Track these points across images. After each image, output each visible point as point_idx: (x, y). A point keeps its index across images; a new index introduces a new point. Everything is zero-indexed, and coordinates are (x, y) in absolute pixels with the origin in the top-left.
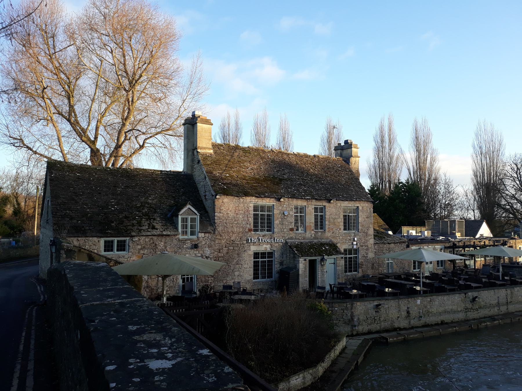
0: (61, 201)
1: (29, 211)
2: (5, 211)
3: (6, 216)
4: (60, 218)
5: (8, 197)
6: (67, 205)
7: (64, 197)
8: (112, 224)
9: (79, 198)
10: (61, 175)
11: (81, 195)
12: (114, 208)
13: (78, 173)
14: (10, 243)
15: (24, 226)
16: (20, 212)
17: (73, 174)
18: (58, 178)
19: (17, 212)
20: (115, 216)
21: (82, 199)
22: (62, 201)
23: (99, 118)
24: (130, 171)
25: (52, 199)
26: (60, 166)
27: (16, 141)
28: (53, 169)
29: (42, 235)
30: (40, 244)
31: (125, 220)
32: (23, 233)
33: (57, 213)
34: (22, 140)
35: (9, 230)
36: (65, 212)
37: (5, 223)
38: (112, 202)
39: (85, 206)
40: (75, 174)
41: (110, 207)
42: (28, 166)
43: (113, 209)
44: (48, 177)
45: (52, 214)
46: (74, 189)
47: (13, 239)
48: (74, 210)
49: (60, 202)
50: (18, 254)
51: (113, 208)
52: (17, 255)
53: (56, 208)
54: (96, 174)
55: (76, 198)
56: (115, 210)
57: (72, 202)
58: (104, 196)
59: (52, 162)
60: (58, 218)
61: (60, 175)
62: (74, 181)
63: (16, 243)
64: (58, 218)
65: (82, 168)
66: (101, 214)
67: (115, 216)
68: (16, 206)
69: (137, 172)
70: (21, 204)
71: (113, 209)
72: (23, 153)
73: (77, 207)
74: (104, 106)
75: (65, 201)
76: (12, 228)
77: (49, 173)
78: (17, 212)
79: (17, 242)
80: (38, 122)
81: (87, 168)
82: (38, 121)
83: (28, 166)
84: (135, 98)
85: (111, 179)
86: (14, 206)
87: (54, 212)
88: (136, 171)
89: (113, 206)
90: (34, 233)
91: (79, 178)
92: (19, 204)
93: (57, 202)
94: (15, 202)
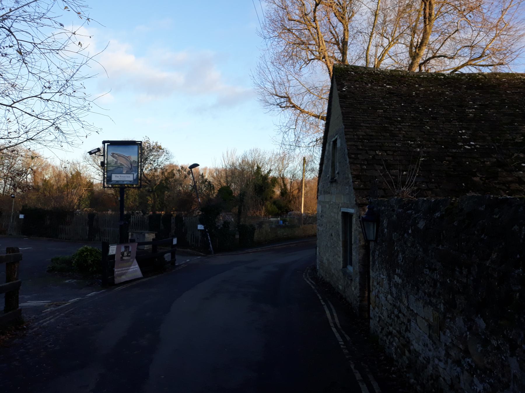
0: (364, 134)
1: (294, 192)
2: (273, 192)
3: (275, 197)
4: (364, 164)
5: (276, 179)
6: (375, 141)
7: (369, 125)
8: (475, 179)
9: (397, 128)
10: (359, 87)
11: (400, 122)
12: (470, 145)
13: (388, 84)
14: (278, 222)
15: (289, 206)
16: (286, 193)
17: (380, 86)
18: (353, 93)
19: (284, 193)
20: (476, 161)
21: (403, 129)
22: (365, 132)
23: (376, 64)
24: (482, 78)
25: (346, 130)
26: (355, 73)
27: (282, 100)
28: (344, 80)
29: (322, 207)
30: (318, 221)
31: (499, 170)
32: (289, 213)
33: (359, 156)
34: (288, 97)
35: (277, 210)
36: (373, 153)
37: (275, 203)
38: (463, 134)
39: (411, 141)
40: (383, 86)
41: (460, 144)
42: (295, 129)
43: (467, 147)
44: (336, 93)
45: (350, 158)
46: (384, 111)
47: (280, 219)
48: (390, 150)
49: (363, 135)
50: (285, 234)
51: (468, 146)
52: (285, 235)
53: (356, 146)
54: (420, 85)
55: (392, 127)
56: (472, 149)
57: (385, 134)
58: (443, 123)
59: (341, 68)
60: (361, 165)
61: (356, 88)
62: (383, 98)
63: (283, 223)
64: (361, 165)
65: (393, 76)
66: (447, 158)
67: (476, 161)
68: (283, 187)
69: (497, 79)
70: (287, 185)
71: (467, 147)
72: (289, 113)
73: (395, 143)
74: (381, 50)
75: (371, 134)
76: (280, 208)
77: (338, 84)
78: (284, 193)
79: (284, 221)
80: (308, 64)
81: (402, 77)
82: (307, 63)
83: (295, 129)
84: (434, 12)
85: (450, 93)
86: (281, 187)
87: (353, 154)
88: (495, 78)
89: (466, 142)
90: (301, 212)
91: (389, 92)
92: (285, 185)
93: (357, 135)
94: (282, 183)
